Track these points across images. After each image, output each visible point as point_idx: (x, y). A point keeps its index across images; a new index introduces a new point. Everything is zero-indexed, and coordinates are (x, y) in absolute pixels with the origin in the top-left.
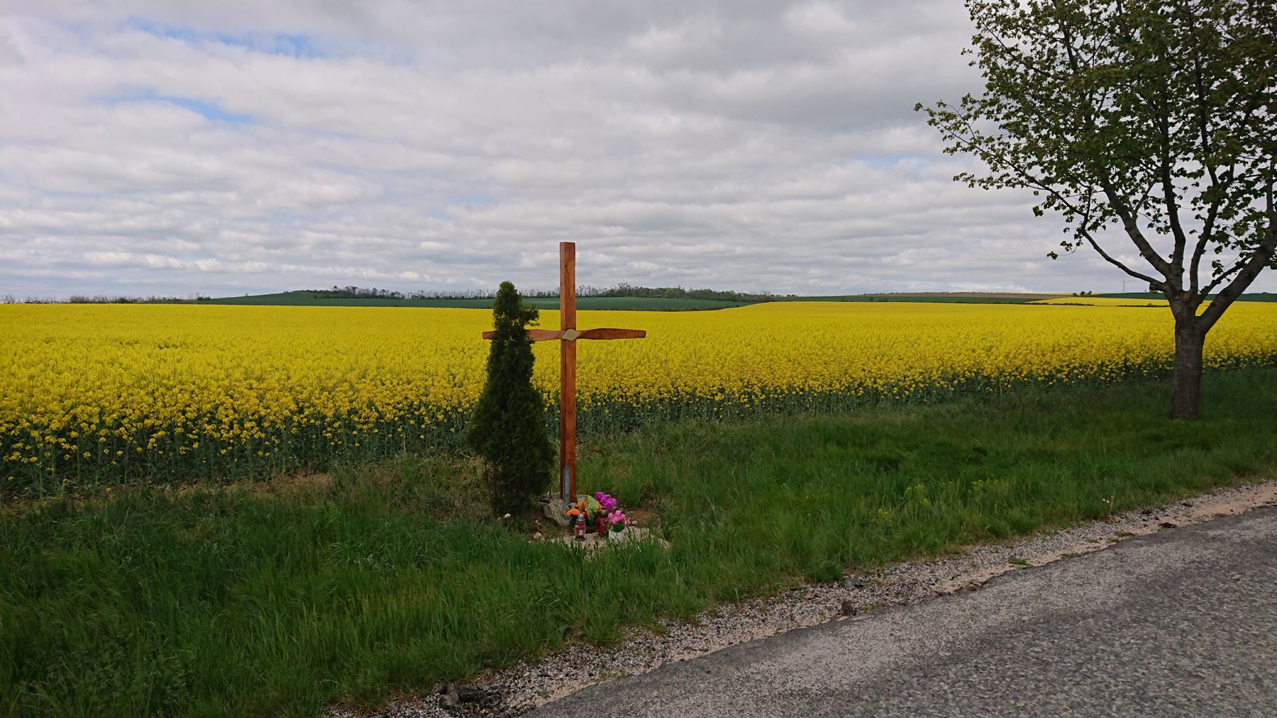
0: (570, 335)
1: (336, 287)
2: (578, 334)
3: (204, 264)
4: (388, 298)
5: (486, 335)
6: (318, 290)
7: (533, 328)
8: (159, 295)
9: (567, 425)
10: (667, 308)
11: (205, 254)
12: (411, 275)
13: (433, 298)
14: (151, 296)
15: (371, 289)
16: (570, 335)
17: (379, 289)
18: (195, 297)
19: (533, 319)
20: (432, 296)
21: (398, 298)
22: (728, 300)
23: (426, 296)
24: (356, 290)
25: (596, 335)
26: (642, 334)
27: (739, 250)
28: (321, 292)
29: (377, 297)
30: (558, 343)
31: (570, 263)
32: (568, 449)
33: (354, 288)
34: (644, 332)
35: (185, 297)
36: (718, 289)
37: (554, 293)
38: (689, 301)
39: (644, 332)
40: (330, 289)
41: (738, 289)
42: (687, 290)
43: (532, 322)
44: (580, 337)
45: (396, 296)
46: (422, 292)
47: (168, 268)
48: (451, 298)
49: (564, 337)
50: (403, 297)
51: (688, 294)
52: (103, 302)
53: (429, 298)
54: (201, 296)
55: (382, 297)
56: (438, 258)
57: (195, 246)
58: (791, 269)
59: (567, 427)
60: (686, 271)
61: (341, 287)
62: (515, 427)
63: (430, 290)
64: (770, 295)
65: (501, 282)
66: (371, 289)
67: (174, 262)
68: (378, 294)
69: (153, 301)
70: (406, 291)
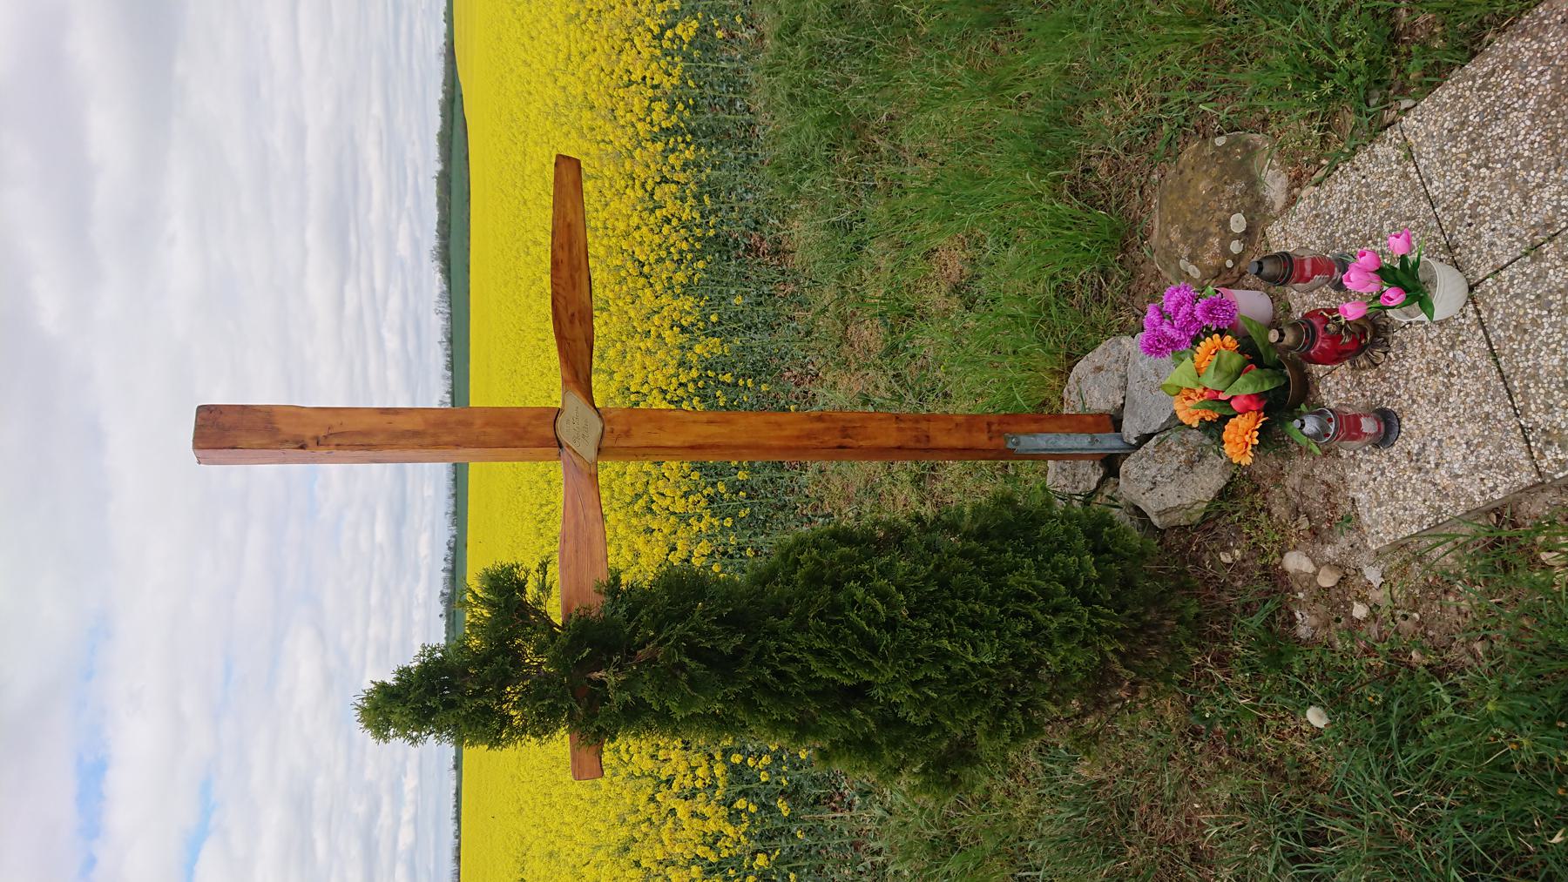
0: (580, 430)
1: (441, 616)
2: (576, 400)
3: (410, 783)
4: (455, 554)
5: (587, 768)
6: (445, 635)
7: (556, 592)
8: (450, 811)
9: (882, 441)
10: (466, 197)
11: (396, 788)
12: (424, 550)
13: (456, 501)
14: (452, 822)
15: (444, 574)
16: (580, 430)
17: (443, 565)
18: (454, 773)
19: (521, 587)
20: (452, 501)
21: (456, 542)
22: (452, 109)
23: (452, 509)
24: (445, 591)
25: (578, 331)
26: (568, 171)
27: (377, 109)
28: (447, 633)
29: (454, 567)
30: (608, 470)
31: (287, 428)
32: (956, 441)
33: (443, 594)
34: (562, 160)
35: (454, 783)
36: (436, 123)
37: (446, 349)
38: (455, 162)
39: (562, 160)
40: (443, 622)
41: (436, 94)
42: (439, 167)
43: (531, 589)
44: (588, 395)
45: (452, 545)
46: (447, 513)
47: (415, 820)
48: (455, 480)
49: (589, 452)
50: (454, 536)
51: (445, 166)
52: (458, 848)
53: (456, 506)
54: (452, 766)
55: (454, 561)
56: (399, 519)
57: (386, 808)
58: (404, 28)
59: (892, 443)
60: (410, 181)
61: (441, 609)
62: (940, 656)
63: (444, 504)
64: (444, 47)
65: (366, 737)
66: (444, 574)
67: (406, 815)
68: (450, 566)
69: (458, 819)
70: (445, 532)
